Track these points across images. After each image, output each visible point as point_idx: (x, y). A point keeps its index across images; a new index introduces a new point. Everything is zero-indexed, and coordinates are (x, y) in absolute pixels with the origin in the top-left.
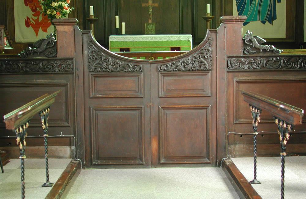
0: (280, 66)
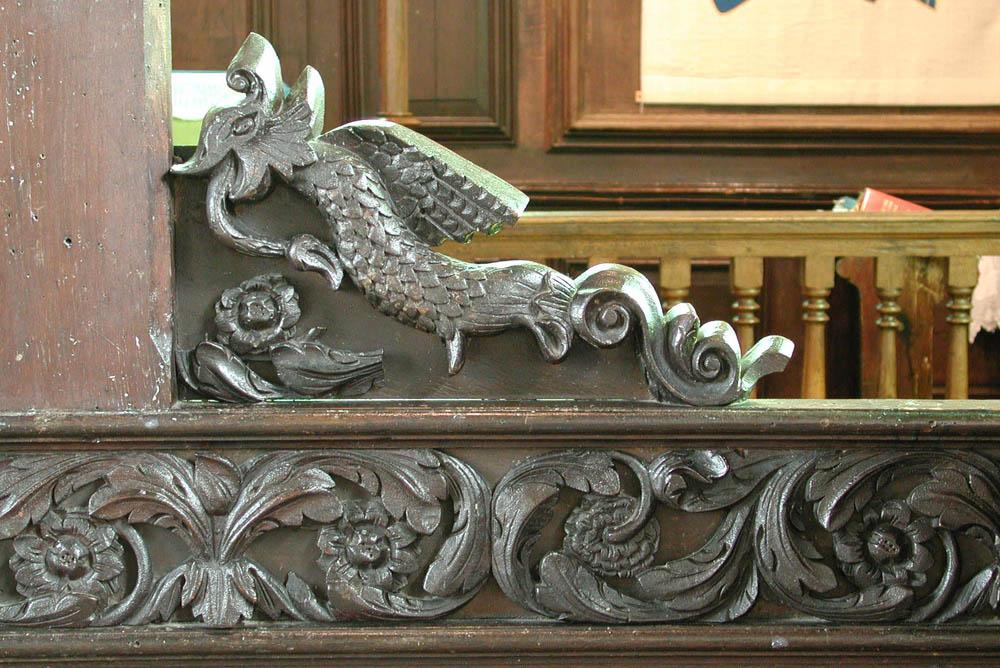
0: (736, 590)
